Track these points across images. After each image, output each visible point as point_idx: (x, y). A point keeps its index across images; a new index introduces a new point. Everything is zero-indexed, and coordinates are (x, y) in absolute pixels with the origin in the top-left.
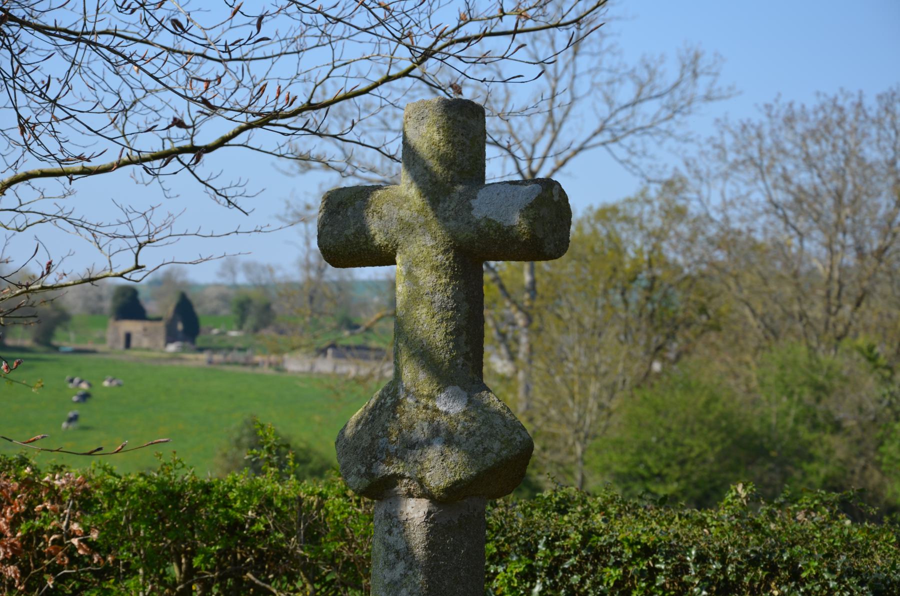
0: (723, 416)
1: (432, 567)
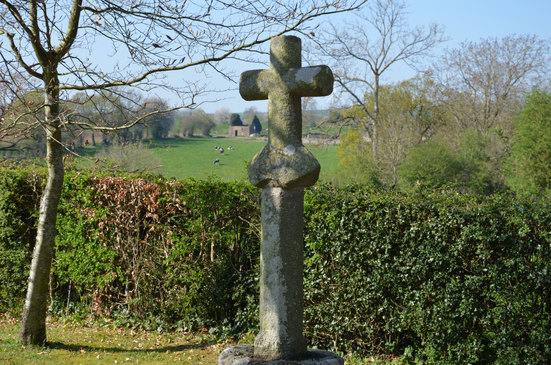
0: (447, 156)
1: (283, 214)
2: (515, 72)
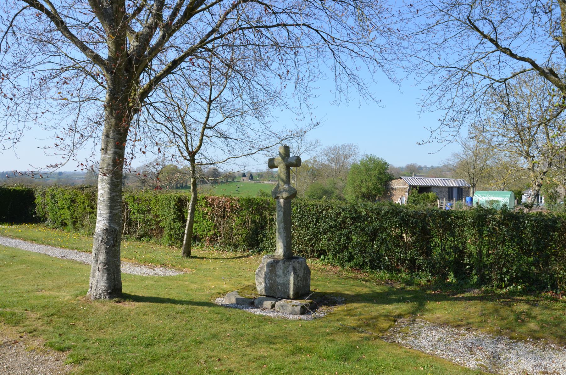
2: (346, 157)
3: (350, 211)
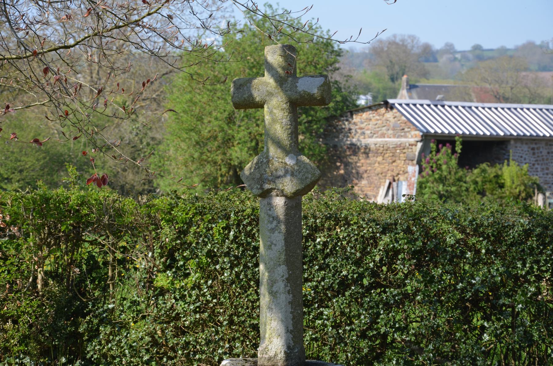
3: (408, 231)
